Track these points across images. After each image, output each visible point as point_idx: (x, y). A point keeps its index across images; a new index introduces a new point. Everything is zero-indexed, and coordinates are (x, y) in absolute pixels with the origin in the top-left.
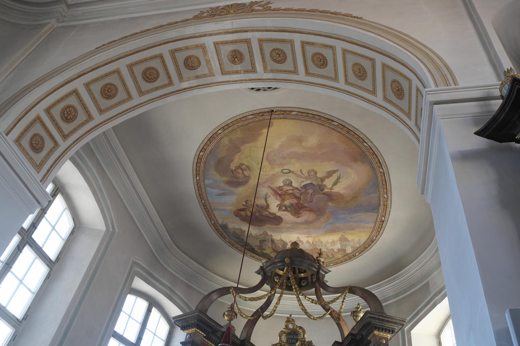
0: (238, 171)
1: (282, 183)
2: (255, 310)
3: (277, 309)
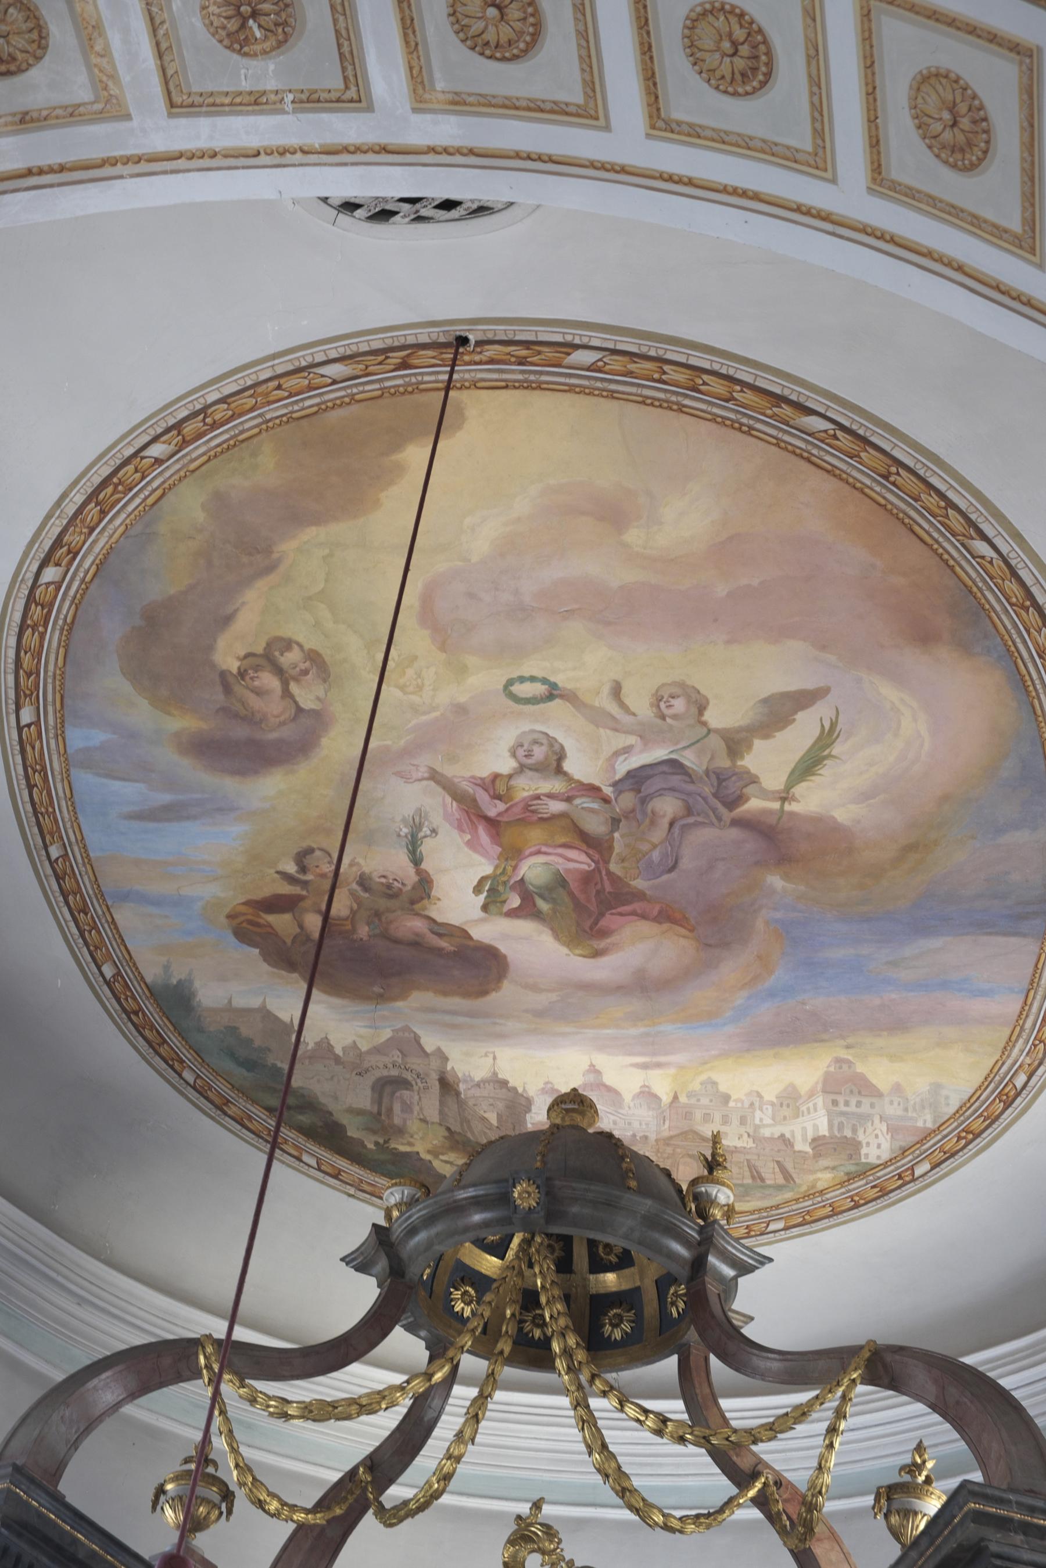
0: (256, 683)
1: (507, 754)
2: (335, 1477)
3: (461, 1468)
